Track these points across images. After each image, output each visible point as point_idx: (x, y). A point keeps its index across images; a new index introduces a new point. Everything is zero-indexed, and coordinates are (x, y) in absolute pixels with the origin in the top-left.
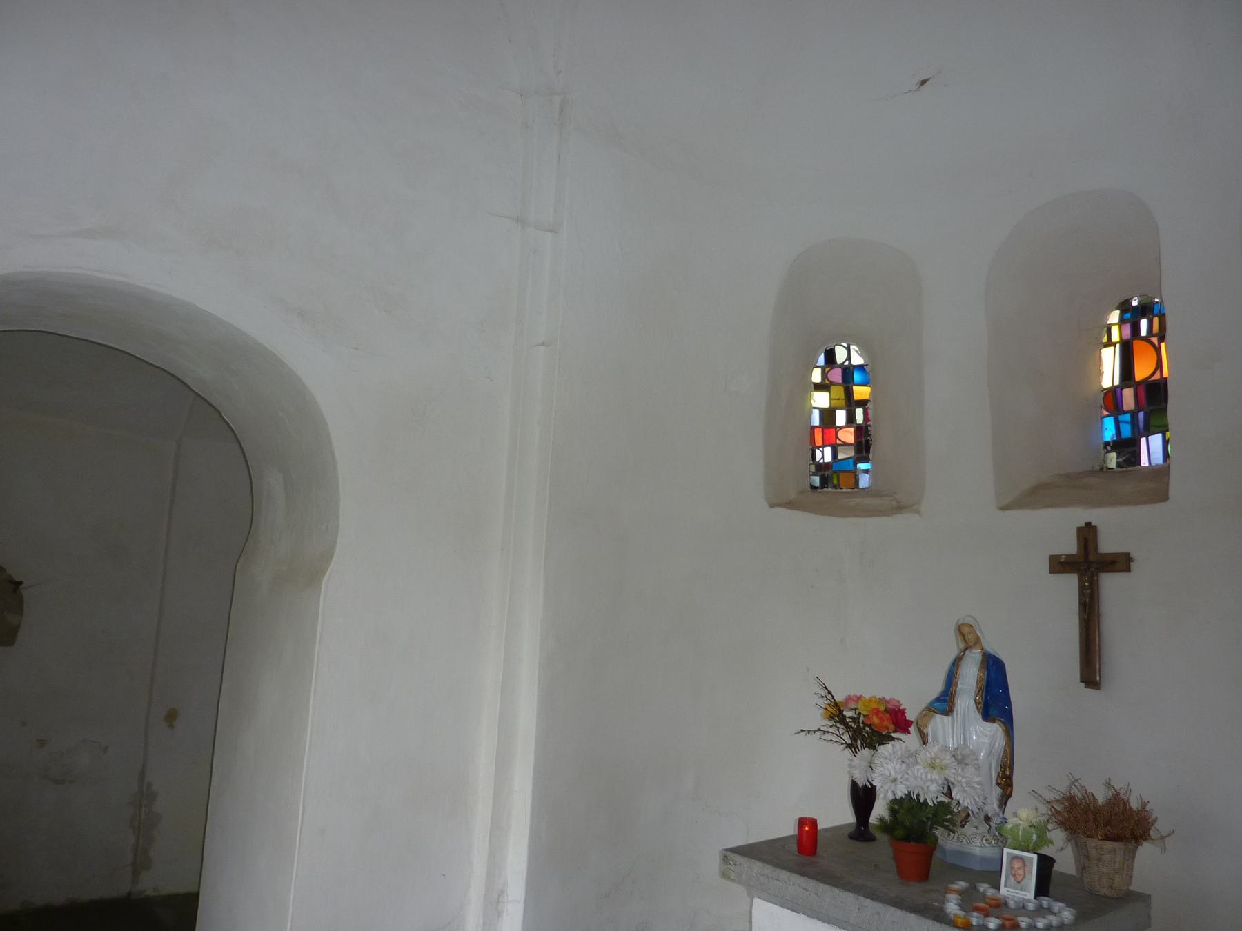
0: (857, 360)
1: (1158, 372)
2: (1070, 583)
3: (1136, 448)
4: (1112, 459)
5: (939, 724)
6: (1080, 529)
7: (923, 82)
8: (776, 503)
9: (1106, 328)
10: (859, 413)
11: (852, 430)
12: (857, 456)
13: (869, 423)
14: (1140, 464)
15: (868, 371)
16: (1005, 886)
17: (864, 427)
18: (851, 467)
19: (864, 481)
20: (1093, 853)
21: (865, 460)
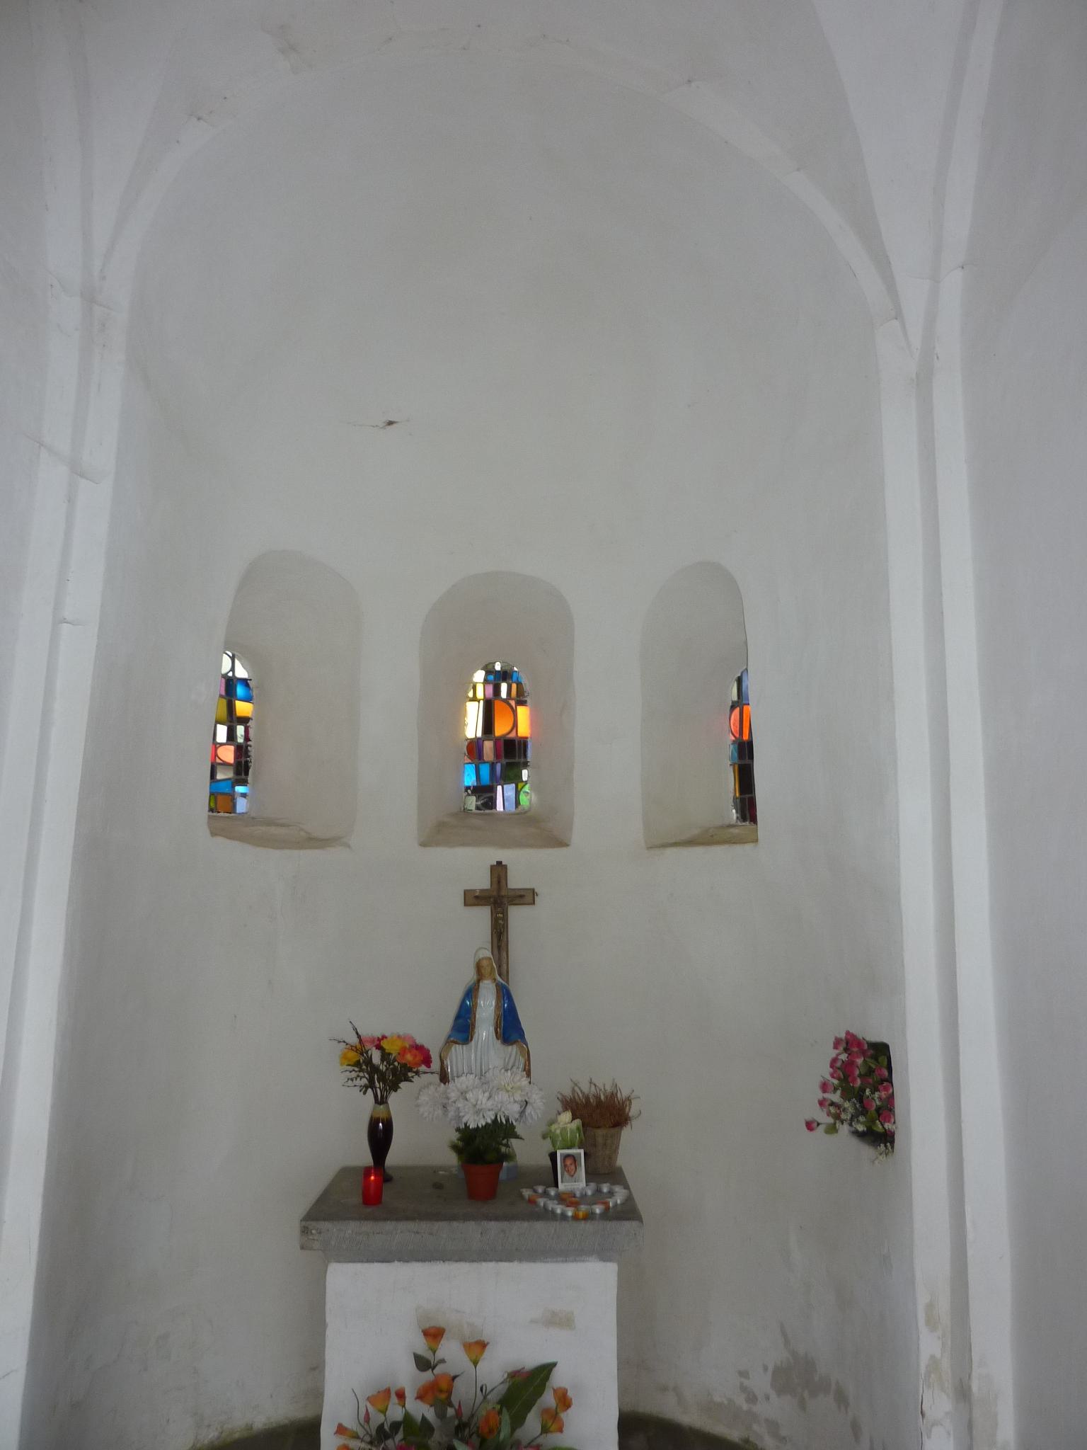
0: (241, 673)
1: (514, 731)
2: (483, 915)
3: (493, 795)
4: (472, 802)
5: (459, 1057)
6: (492, 867)
7: (390, 423)
8: (424, 844)
9: (472, 684)
10: (240, 730)
11: (232, 748)
12: (236, 777)
13: (249, 743)
14: (495, 808)
15: (251, 687)
16: (562, 1182)
17: (244, 747)
18: (227, 790)
19: (242, 805)
20: (600, 1140)
21: (244, 782)
